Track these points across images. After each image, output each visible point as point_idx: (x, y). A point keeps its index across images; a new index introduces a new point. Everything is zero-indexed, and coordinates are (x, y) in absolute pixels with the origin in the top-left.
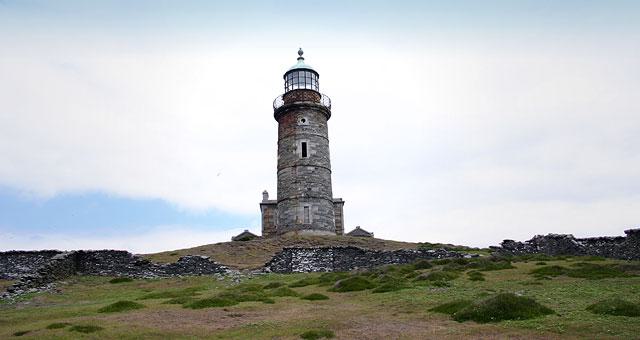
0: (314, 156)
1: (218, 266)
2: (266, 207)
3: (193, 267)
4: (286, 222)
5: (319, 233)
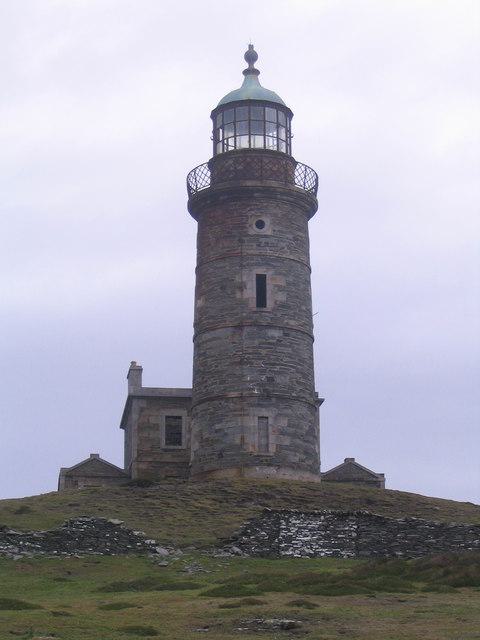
0: (283, 306)
1: (140, 538)
2: (143, 404)
3: (93, 540)
4: (218, 447)
5: (287, 475)
